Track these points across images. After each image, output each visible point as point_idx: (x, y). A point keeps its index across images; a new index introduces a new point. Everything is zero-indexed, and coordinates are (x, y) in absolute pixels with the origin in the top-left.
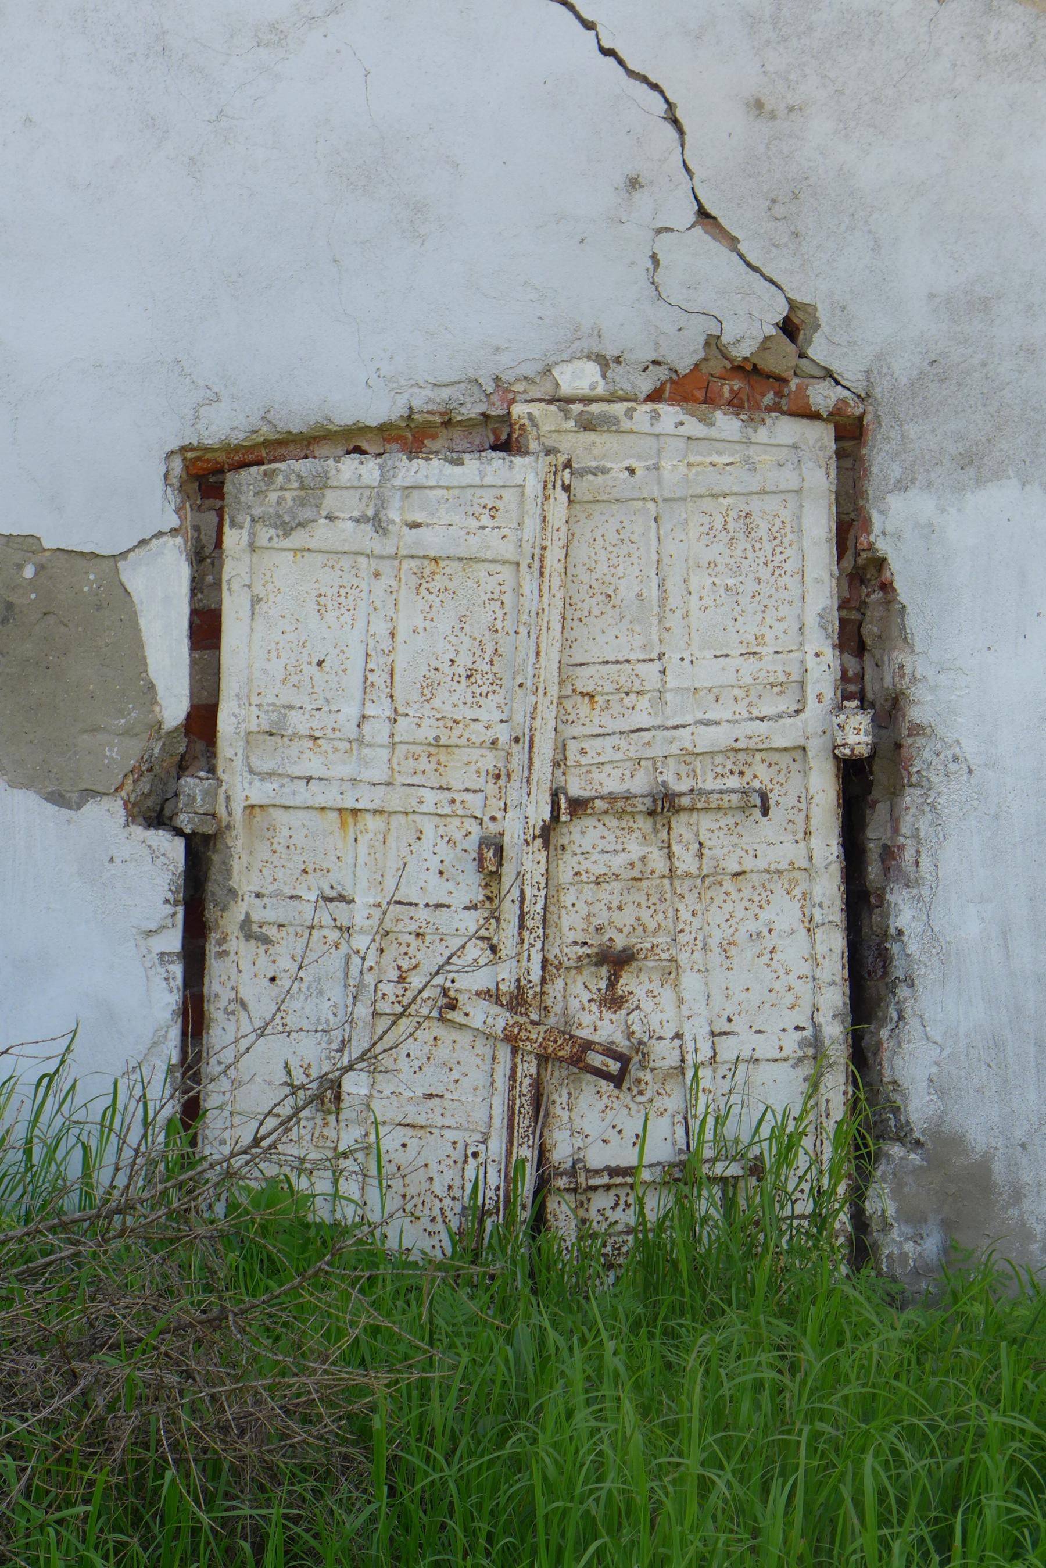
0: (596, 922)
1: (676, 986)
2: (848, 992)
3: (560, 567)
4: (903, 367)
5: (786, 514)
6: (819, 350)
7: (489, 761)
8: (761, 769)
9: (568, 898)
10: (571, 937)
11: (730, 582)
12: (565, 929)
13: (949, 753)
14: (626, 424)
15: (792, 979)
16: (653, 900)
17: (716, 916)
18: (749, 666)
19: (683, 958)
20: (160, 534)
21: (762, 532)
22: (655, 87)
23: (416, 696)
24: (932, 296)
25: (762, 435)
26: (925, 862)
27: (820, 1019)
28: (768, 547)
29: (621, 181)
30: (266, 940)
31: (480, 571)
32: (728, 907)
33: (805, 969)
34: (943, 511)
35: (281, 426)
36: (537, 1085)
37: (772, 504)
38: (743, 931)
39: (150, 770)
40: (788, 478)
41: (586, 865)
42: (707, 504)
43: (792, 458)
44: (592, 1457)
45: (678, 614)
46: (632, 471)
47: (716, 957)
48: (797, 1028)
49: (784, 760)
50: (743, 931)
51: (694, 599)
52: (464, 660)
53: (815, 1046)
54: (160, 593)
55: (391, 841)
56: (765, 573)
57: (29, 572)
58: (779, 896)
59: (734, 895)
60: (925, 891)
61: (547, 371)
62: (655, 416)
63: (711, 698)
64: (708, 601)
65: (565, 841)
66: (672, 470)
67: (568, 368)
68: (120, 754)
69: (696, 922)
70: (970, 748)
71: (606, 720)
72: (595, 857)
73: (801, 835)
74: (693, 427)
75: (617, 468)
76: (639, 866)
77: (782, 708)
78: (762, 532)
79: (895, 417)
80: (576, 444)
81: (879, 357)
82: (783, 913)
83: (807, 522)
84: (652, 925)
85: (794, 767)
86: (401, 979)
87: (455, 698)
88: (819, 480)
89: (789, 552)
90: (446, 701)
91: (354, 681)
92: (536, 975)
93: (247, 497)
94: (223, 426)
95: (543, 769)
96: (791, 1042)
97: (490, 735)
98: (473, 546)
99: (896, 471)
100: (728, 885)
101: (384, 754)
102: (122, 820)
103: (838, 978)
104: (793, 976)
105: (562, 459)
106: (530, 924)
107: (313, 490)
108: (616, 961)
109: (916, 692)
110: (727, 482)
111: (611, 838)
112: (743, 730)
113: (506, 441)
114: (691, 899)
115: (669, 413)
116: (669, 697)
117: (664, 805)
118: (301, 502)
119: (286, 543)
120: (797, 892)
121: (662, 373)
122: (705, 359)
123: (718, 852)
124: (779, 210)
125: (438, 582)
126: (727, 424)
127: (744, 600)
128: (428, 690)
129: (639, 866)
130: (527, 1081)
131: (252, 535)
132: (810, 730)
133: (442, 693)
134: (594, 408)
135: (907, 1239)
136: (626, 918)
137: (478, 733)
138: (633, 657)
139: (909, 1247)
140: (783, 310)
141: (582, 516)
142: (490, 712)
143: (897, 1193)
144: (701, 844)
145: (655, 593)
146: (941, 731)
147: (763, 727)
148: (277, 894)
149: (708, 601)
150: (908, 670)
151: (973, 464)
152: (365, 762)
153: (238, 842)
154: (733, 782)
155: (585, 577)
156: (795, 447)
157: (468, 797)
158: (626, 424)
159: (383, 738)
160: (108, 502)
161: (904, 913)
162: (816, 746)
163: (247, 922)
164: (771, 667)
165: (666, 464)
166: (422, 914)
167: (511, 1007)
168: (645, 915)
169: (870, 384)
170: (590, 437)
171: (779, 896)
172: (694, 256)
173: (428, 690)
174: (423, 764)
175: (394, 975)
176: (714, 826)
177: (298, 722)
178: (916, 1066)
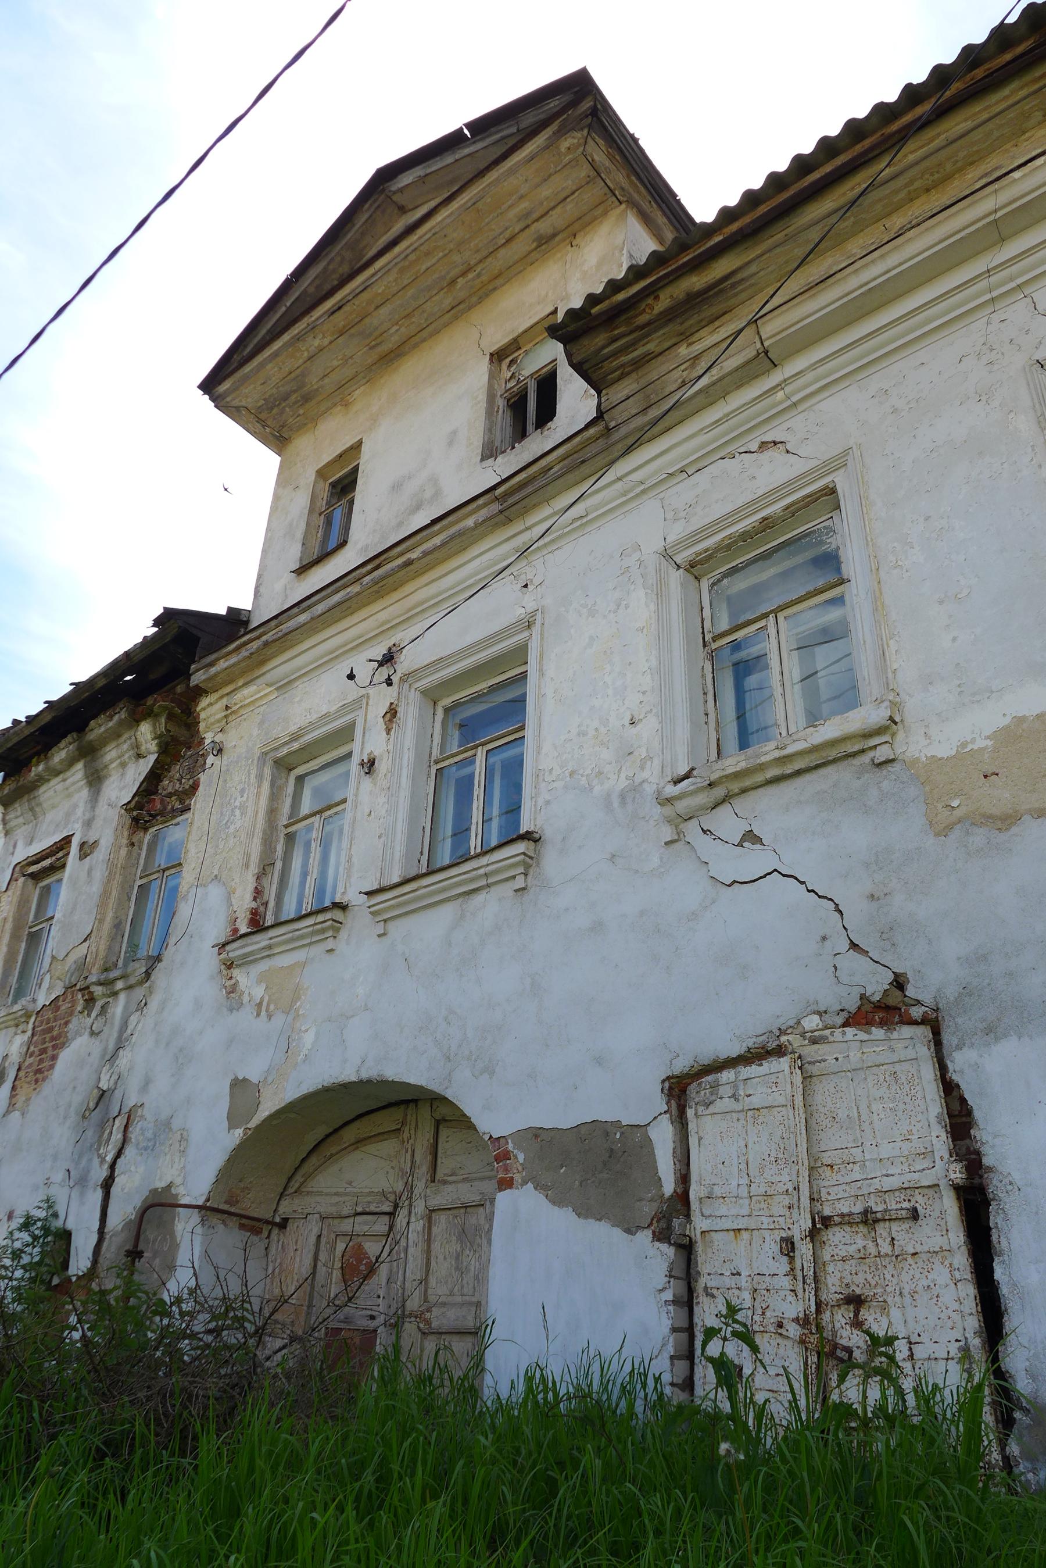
0: (846, 1281)
1: (888, 1316)
2: (982, 1319)
3: (802, 1104)
4: (951, 993)
5: (913, 1071)
6: (910, 992)
7: (787, 1201)
8: (919, 1198)
9: (830, 1268)
10: (833, 1289)
11: (891, 1106)
12: (830, 1285)
13: (1007, 1180)
14: (831, 1039)
15: (950, 1312)
16: (873, 1269)
17: (905, 1277)
18: (906, 1146)
19: (889, 1300)
20: (660, 1114)
21: (903, 1080)
22: (831, 900)
23: (758, 1173)
24: (959, 959)
25: (895, 1035)
26: (1003, 1240)
27: (967, 1335)
28: (907, 1087)
29: (819, 939)
30: (713, 1296)
31: (775, 1111)
32: (911, 1272)
33: (956, 1306)
34: (981, 1056)
35: (701, 1063)
36: (818, 1367)
37: (906, 1066)
38: (920, 1285)
39: (664, 1217)
40: (910, 1053)
41: (836, 1251)
42: (875, 1070)
43: (910, 1043)
44: (68, 1453)
45: (867, 1123)
46: (837, 1059)
47: (908, 1300)
48: (957, 1340)
49: (931, 1192)
50: (920, 1285)
51: (875, 1114)
52: (773, 1154)
53: (965, 1350)
54: (663, 1137)
55: (754, 1244)
56: (907, 1100)
57: (618, 1136)
58: (937, 1266)
59: (914, 1266)
60: (1006, 1258)
61: (799, 1023)
62: (844, 1033)
63: (889, 1163)
64: (882, 1116)
65: (825, 1239)
66: (855, 1055)
67: (807, 1019)
68: (648, 1209)
69: (895, 1281)
70: (1016, 1176)
71: (839, 1177)
72: (841, 1247)
73: (945, 1232)
74: (862, 1036)
75: (831, 1059)
76: (862, 1251)
77: (925, 1166)
78: (903, 1080)
79: (951, 1016)
80: (810, 1052)
81: (939, 990)
82: (941, 1275)
83: (923, 1073)
84: (873, 1283)
85: (936, 1195)
86: (763, 1313)
87: (772, 1172)
88: (925, 1053)
89: (917, 1088)
90: (770, 1173)
91: (735, 1170)
92: (813, 1308)
93: (693, 1095)
94: (681, 1066)
95: (805, 1201)
96: (954, 1349)
97: (785, 1188)
98: (770, 1101)
99: (955, 1041)
100: (910, 1260)
101: (747, 1201)
102: (651, 1239)
103: (974, 1311)
104: (950, 1310)
105: (797, 1055)
106: (808, 1281)
107: (715, 1086)
108: (856, 1301)
109: (984, 1150)
110: (881, 1059)
111: (848, 1237)
112: (904, 1178)
113: (780, 1051)
114: (890, 1267)
115: (850, 1031)
116: (867, 1163)
117: (869, 1219)
118: (712, 1094)
119: (708, 1112)
120: (947, 1263)
121: (845, 1014)
122: (862, 1005)
123: (902, 1243)
124: (884, 936)
125: (760, 1121)
126: (878, 1033)
127: (900, 1113)
128: (762, 1169)
129: (862, 1251)
130: (814, 1366)
131: (696, 1110)
132: (939, 1176)
133: (767, 1170)
134: (816, 1033)
135: (1029, 1471)
136: (860, 1279)
137: (782, 1188)
138: (849, 1146)
139: (1030, 1476)
140: (891, 977)
141: (817, 1082)
142: (785, 1178)
143: (1019, 1444)
144: (893, 1239)
145: (856, 1115)
146: (1000, 1168)
147: (916, 1176)
148: (716, 1273)
149: (882, 1116)
150: (978, 1138)
151: (992, 1032)
152: (741, 1207)
153: (699, 1248)
154: (906, 1205)
155: (822, 1110)
156: (912, 1038)
157: (780, 1219)
158: (831, 1039)
159: (746, 1194)
160: (637, 1102)
161: (999, 1273)
162: (943, 1183)
163: (706, 1288)
164: (917, 1145)
165: (851, 1054)
166: (767, 1279)
167: (803, 1326)
168: (869, 1277)
169: (937, 1004)
170: (816, 1046)
171: (937, 1266)
172: (854, 966)
173: (762, 1169)
174: (763, 1205)
175: (760, 1312)
176: (899, 1229)
177: (718, 1191)
178: (1017, 1360)
